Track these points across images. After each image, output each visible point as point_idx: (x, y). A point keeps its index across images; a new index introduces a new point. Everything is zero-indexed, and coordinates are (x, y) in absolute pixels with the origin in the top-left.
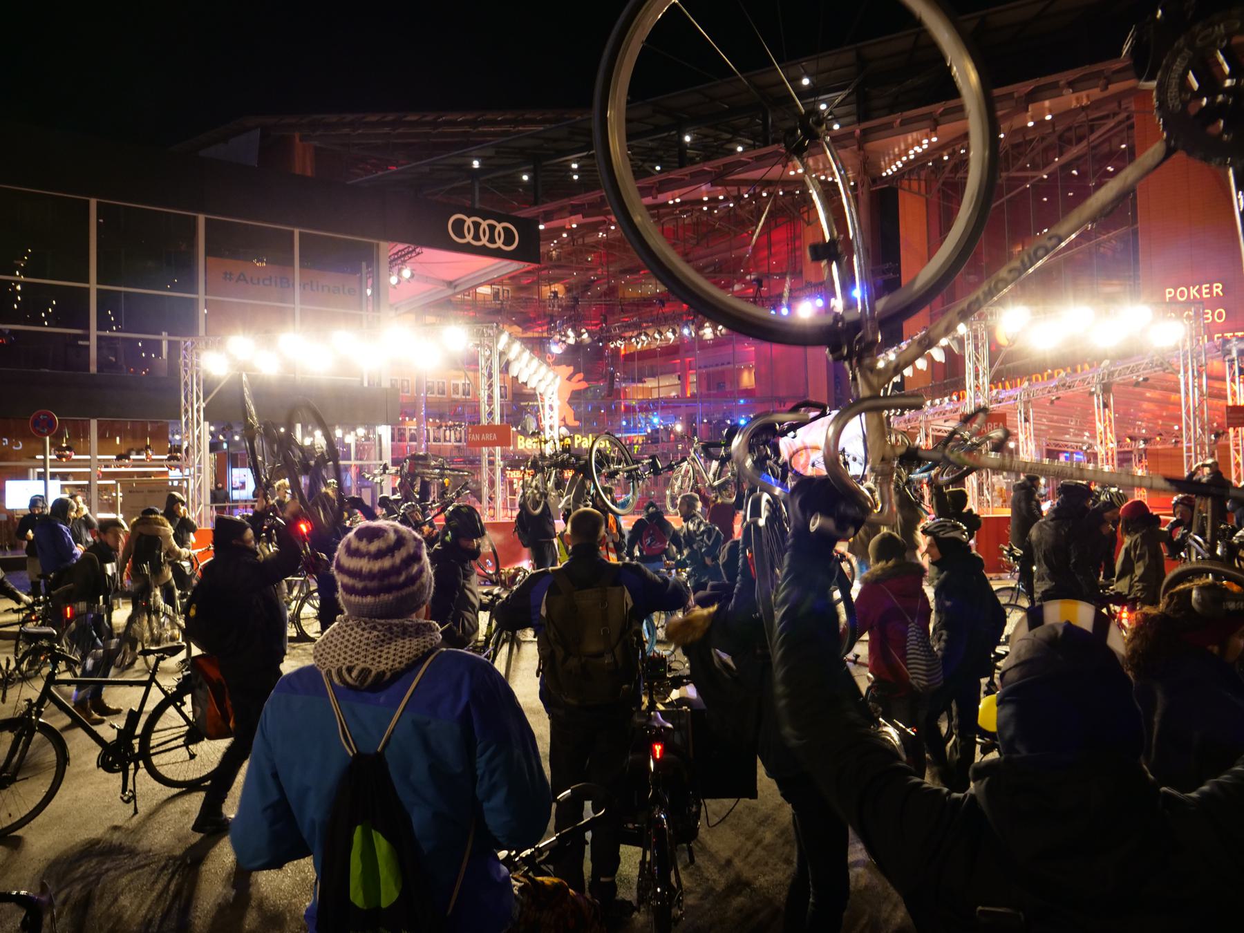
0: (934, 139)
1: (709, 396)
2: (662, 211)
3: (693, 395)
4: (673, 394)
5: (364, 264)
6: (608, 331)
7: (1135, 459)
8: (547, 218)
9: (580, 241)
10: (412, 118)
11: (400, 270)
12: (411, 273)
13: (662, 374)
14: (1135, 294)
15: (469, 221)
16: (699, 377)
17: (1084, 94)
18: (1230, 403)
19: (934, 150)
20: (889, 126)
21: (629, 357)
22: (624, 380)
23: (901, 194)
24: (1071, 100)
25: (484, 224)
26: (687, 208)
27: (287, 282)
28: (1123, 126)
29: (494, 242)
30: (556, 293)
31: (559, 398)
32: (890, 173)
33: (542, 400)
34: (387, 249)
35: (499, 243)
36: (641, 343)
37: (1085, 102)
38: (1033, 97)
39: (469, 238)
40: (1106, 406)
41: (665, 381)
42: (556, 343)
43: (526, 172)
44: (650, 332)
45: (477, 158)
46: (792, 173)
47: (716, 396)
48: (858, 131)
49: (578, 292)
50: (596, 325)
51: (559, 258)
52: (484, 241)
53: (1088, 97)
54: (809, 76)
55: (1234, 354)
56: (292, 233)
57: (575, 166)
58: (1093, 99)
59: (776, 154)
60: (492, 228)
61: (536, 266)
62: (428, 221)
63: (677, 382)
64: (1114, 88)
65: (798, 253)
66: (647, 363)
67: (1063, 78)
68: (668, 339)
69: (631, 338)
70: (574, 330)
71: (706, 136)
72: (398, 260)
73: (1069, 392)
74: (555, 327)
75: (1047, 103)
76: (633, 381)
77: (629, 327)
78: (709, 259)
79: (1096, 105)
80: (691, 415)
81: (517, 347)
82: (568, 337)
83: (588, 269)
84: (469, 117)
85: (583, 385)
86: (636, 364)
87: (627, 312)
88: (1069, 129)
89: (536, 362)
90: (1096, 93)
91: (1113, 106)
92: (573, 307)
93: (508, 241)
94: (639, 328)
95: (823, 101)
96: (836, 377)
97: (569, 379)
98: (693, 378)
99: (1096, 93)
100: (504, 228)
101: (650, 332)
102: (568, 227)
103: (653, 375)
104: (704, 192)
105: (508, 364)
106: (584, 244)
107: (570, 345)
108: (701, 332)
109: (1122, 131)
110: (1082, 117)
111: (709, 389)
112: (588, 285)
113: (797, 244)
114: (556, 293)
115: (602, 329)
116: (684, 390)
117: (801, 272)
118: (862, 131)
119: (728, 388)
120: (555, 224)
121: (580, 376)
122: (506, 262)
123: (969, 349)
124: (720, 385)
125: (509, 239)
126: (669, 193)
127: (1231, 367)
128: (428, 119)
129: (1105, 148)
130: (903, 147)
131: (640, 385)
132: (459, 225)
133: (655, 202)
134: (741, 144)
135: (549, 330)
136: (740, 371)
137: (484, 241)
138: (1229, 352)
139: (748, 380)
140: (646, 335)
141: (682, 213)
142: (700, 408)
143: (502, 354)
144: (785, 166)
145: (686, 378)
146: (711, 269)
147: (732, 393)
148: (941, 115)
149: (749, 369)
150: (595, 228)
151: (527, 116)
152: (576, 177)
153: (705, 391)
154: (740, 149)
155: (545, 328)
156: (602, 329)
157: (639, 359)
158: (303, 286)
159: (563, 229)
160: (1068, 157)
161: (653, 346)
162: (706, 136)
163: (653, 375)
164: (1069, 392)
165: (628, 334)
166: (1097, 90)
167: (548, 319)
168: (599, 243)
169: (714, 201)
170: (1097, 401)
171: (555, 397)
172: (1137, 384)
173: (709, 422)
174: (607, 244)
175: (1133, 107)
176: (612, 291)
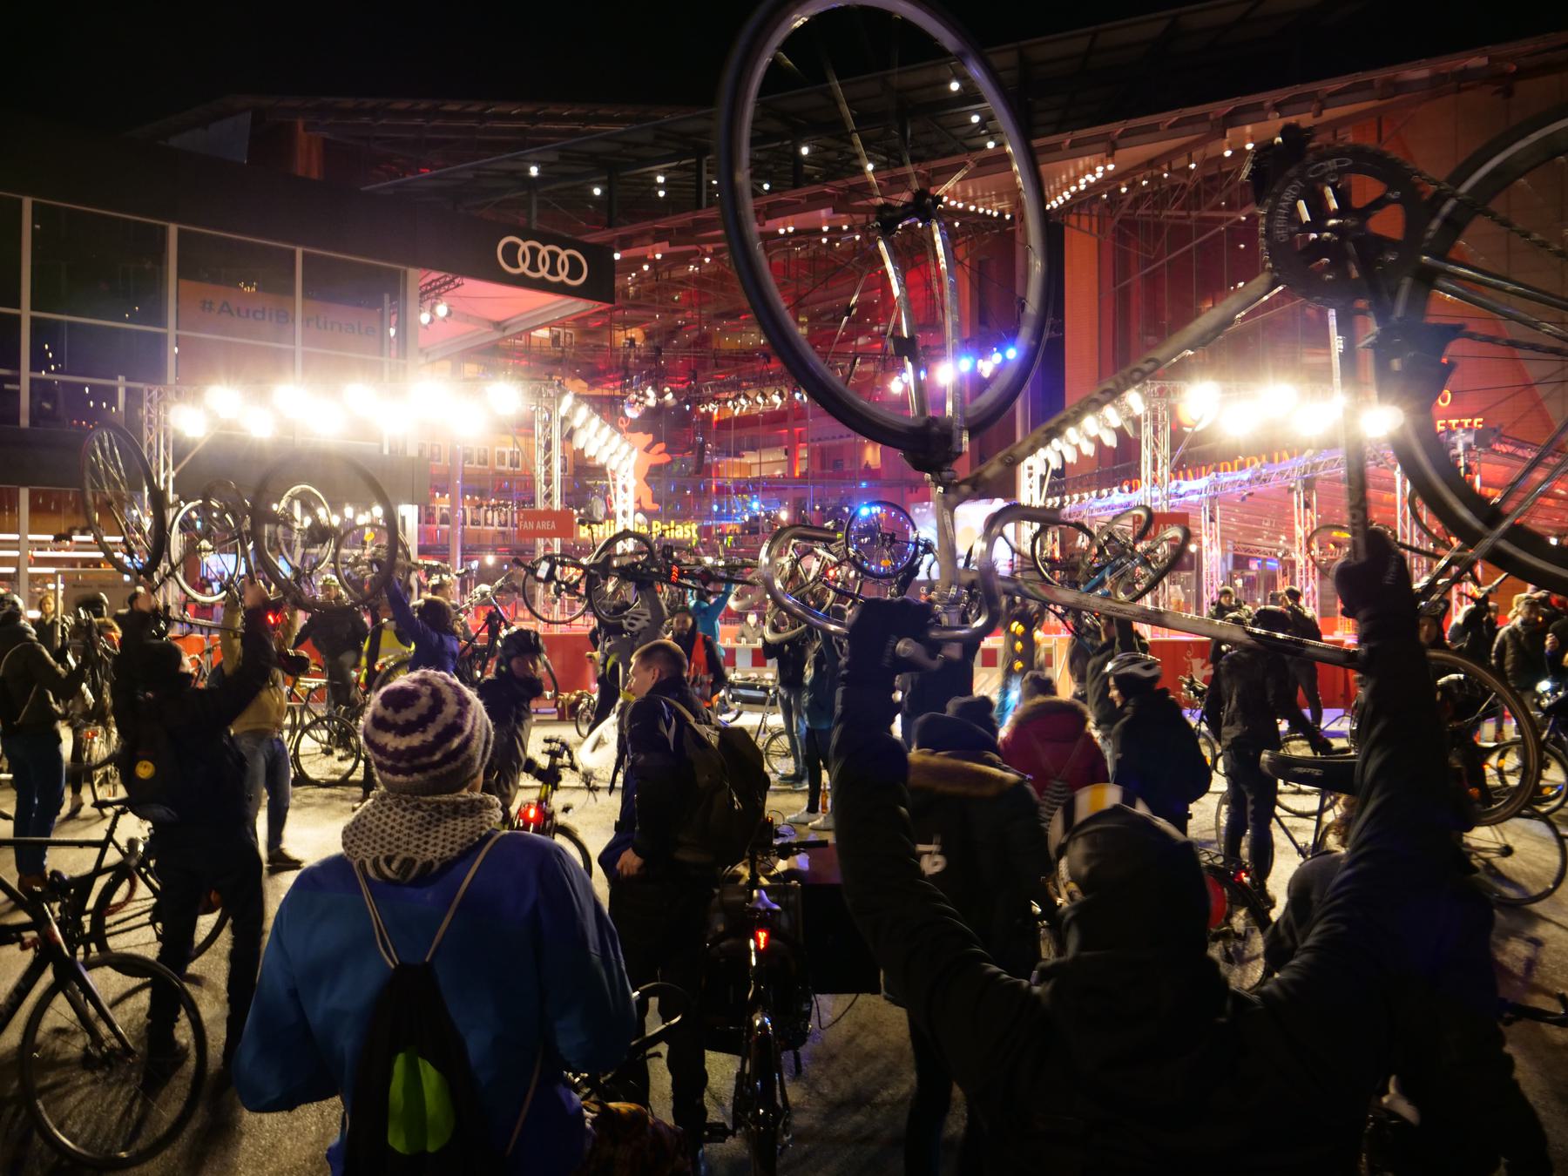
1: (822, 476)
4: (778, 472)
5: (387, 297)
8: (624, 244)
10: (453, 107)
12: (444, 310)
15: (524, 246)
16: (812, 452)
19: (1109, 181)
21: (724, 424)
22: (717, 453)
25: (544, 251)
26: (801, 238)
27: (286, 317)
30: (632, 341)
34: (417, 278)
35: (563, 276)
36: (740, 407)
38: (1232, 120)
39: (524, 268)
40: (1307, 505)
42: (632, 404)
44: (751, 394)
45: (536, 163)
49: (661, 339)
50: (683, 382)
52: (543, 272)
57: (660, 179)
61: (605, 306)
63: (783, 457)
64: (1329, 114)
66: (748, 432)
67: (1268, 98)
68: (772, 404)
69: (727, 400)
70: (655, 388)
72: (430, 293)
74: (631, 384)
75: (1248, 129)
76: (728, 455)
78: (828, 304)
81: (584, 411)
82: (647, 397)
84: (527, 109)
85: (665, 458)
86: (733, 434)
87: (723, 367)
94: (738, 389)
95: (976, 112)
97: (647, 450)
98: (804, 454)
101: (751, 394)
104: (823, 218)
111: (823, 467)
112: (673, 332)
114: (632, 341)
116: (791, 468)
119: (847, 467)
120: (635, 252)
123: (1147, 432)
124: (837, 464)
125: (575, 272)
126: (780, 220)
130: (1072, 173)
131: (737, 460)
132: (511, 251)
135: (623, 387)
137: (543, 272)
140: (747, 397)
143: (564, 420)
147: (851, 474)
148: (1121, 136)
150: (685, 259)
153: (818, 471)
156: (690, 388)
162: (828, 149)
163: (753, 448)
165: (723, 396)
168: (691, 278)
171: (630, 475)
174: (698, 280)
176: (704, 340)
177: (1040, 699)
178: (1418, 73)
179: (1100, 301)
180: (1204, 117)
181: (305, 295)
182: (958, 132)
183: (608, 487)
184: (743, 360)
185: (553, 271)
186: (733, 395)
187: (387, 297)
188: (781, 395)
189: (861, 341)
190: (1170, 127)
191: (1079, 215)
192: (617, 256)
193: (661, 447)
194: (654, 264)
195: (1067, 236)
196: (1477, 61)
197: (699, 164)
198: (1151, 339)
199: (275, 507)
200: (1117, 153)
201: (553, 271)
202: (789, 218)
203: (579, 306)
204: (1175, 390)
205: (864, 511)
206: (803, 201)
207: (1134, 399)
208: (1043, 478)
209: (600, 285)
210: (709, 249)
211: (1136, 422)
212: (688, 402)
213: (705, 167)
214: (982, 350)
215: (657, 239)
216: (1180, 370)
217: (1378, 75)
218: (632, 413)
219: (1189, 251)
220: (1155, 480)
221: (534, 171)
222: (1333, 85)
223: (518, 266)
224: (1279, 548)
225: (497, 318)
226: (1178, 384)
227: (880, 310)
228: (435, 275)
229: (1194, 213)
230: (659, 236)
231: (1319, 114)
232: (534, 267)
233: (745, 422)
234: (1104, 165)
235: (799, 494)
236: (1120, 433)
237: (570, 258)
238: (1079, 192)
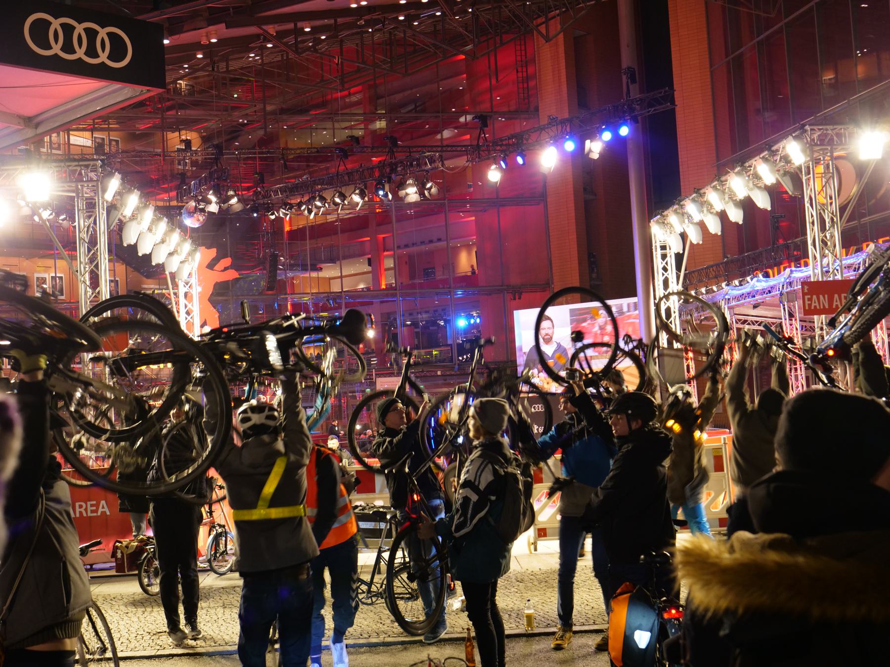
1: (413, 286)
3: (389, 287)
8: (174, 28)
9: (223, 65)
13: (345, 258)
15: (56, 24)
16: (398, 261)
21: (297, 235)
22: (292, 267)
25: (80, 29)
26: (375, 16)
29: (96, 56)
30: (188, 143)
31: (200, 282)
33: (175, 286)
35: (103, 57)
36: (315, 213)
39: (56, 49)
41: (349, 269)
42: (191, 214)
44: (327, 195)
47: (421, 286)
49: (218, 143)
50: (248, 189)
51: (192, 91)
52: (80, 53)
59: (420, 642)
61: (155, 91)
63: (367, 268)
65: (532, 84)
66: (325, 242)
68: (354, 205)
69: (300, 205)
70: (217, 193)
74: (189, 190)
76: (304, 269)
77: (294, 190)
80: (389, 314)
81: (133, 200)
82: (209, 202)
83: (234, 108)
85: (232, 274)
86: (308, 244)
87: (293, 170)
89: (163, 225)
92: (216, 160)
94: (311, 190)
96: (590, 255)
97: (211, 266)
98: (389, 263)
100: (109, 34)
101: (327, 195)
102: (204, 41)
103: (332, 260)
105: (121, 226)
107: (211, 214)
108: (402, 193)
111: (412, 276)
112: (235, 132)
113: (530, 70)
114: (188, 143)
115: (256, 194)
116: (377, 280)
117: (537, 109)
119: (439, 276)
120: (186, 37)
121: (227, 262)
122: (117, 86)
124: (428, 272)
125: (117, 53)
131: (314, 274)
132: (41, 29)
135: (179, 198)
136: (455, 251)
137: (80, 53)
139: (466, 262)
140: (323, 199)
141: (369, 24)
142: (400, 305)
143: (112, 208)
145: (380, 263)
147: (445, 282)
149: (468, 247)
150: (244, 44)
153: (406, 281)
155: (173, 194)
156: (256, 194)
159: (198, 46)
161: (331, 218)
163: (332, 260)
165: (295, 201)
167: (176, 183)
168: (248, 69)
171: (194, 281)
173: (415, 324)
174: (261, 72)
176: (268, 140)
179: (712, 73)
185: (92, 52)
186: (306, 198)
189: (447, 134)
192: (166, 42)
193: (227, 262)
194: (209, 49)
198: (769, 116)
201: (92, 52)
204: (839, 135)
205: (462, 323)
207: (794, 150)
208: (679, 257)
209: (148, 68)
210: (272, 29)
211: (796, 177)
212: (254, 209)
214: (584, 133)
215: (212, 22)
216: (849, 117)
218: (191, 222)
220: (824, 243)
223: (49, 47)
225: (29, 112)
226: (851, 127)
227: (467, 97)
232: (68, 47)
233: (320, 230)
235: (386, 308)
236: (775, 192)
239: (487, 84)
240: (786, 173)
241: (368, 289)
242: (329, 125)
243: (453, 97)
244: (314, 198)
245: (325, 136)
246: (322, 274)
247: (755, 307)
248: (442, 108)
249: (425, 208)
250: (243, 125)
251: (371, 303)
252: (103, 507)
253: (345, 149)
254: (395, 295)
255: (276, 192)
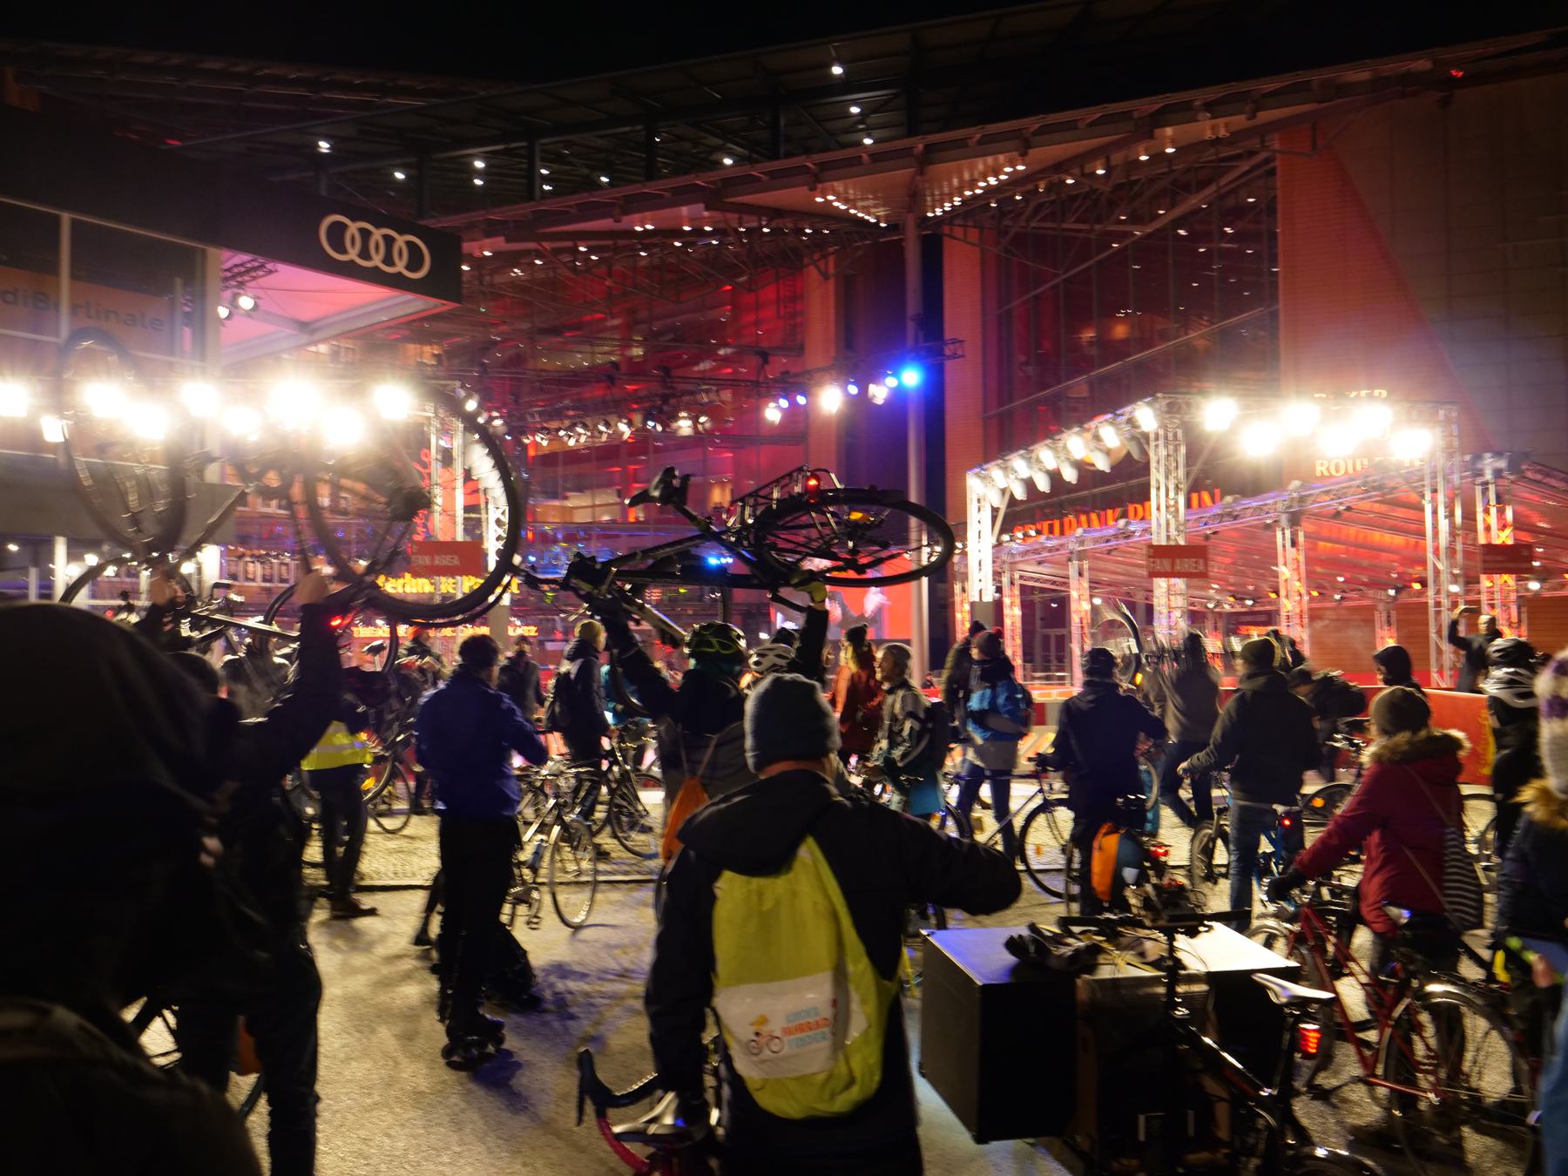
0: (1020, 168)
1: (668, 521)
2: (621, 242)
4: (606, 518)
5: (178, 282)
6: (522, 418)
7: (1379, 617)
10: (214, 65)
11: (235, 297)
12: (256, 299)
14: (1232, 395)
15: (353, 228)
17: (1221, 121)
18: (1482, 540)
19: (1016, 181)
20: (962, 143)
23: (947, 242)
24: (1206, 128)
25: (378, 234)
27: (44, 300)
28: (1261, 171)
32: (939, 212)
34: (225, 259)
35: (400, 267)
37: (1223, 133)
38: (1158, 119)
39: (353, 254)
40: (1294, 544)
43: (401, 168)
45: (326, 138)
46: (819, 200)
48: (921, 146)
52: (377, 261)
53: (1227, 125)
54: (841, 64)
55: (1489, 476)
56: (56, 220)
57: (479, 164)
58: (1234, 128)
60: (389, 241)
61: (449, 306)
62: (283, 220)
64: (1264, 116)
67: (1199, 96)
71: (681, 138)
72: (237, 279)
73: (1237, 524)
75: (1169, 131)
78: (669, 321)
79: (1237, 136)
84: (307, 73)
86: (560, 470)
88: (1189, 170)
90: (1239, 121)
91: (1255, 143)
93: (415, 264)
95: (855, 103)
99: (1239, 121)
102: (477, 254)
104: (687, 217)
106: (492, 285)
108: (675, 425)
109: (1259, 177)
110: (1209, 155)
118: (926, 146)
122: (408, 296)
123: (1157, 454)
125: (415, 262)
126: (637, 216)
127: (1485, 491)
128: (240, 69)
129: (1231, 202)
130: (967, 176)
131: (557, 503)
132: (337, 232)
133: (618, 227)
134: (730, 155)
137: (377, 261)
138: (1480, 473)
144: (813, 189)
146: (671, 336)
148: (1035, 134)
149: (722, 484)
151: (401, 82)
152: (478, 182)
154: (728, 161)
157: (565, 464)
158: (74, 309)
160: (1178, 211)
162: (681, 138)
164: (1237, 524)
165: (554, 425)
166: (1242, 117)
168: (515, 284)
169: (698, 232)
170: (1282, 538)
172: (1337, 514)
175: (1277, 146)
176: (517, 360)
177: (1402, 737)
178: (1358, 75)
179: (984, 324)
180: (1127, 115)
181: (74, 277)
182: (839, 124)
183: (479, 520)
184: (572, 384)
186: (567, 423)
187: (178, 282)
188: (630, 424)
190: (1091, 125)
191: (965, 226)
195: (946, 251)
196: (1422, 64)
197: (530, 148)
199: (626, 436)
200: (1031, 151)
202: (648, 214)
203: (413, 304)
204: (1188, 405)
206: (573, 211)
207: (1146, 416)
208: (995, 510)
210: (547, 245)
213: (538, 155)
215: (489, 234)
217: (1316, 77)
219: (1089, 268)
221: (324, 146)
222: (1269, 85)
223: (344, 251)
224: (1210, 599)
228: (245, 257)
229: (1097, 227)
230: (491, 230)
231: (1253, 116)
232: (365, 254)
234: (1012, 164)
237: (410, 244)
238: (975, 197)
239: (753, 317)
240: (1133, 438)
241: (613, 521)
242: (588, 348)
243: (715, 328)
244: (575, 425)
245: (581, 360)
246: (569, 504)
247: (1040, 563)
248: (701, 338)
249: (698, 439)
250: (496, 343)
251: (617, 536)
252: (833, 702)
253: (609, 375)
254: (647, 530)
255: (532, 416)
